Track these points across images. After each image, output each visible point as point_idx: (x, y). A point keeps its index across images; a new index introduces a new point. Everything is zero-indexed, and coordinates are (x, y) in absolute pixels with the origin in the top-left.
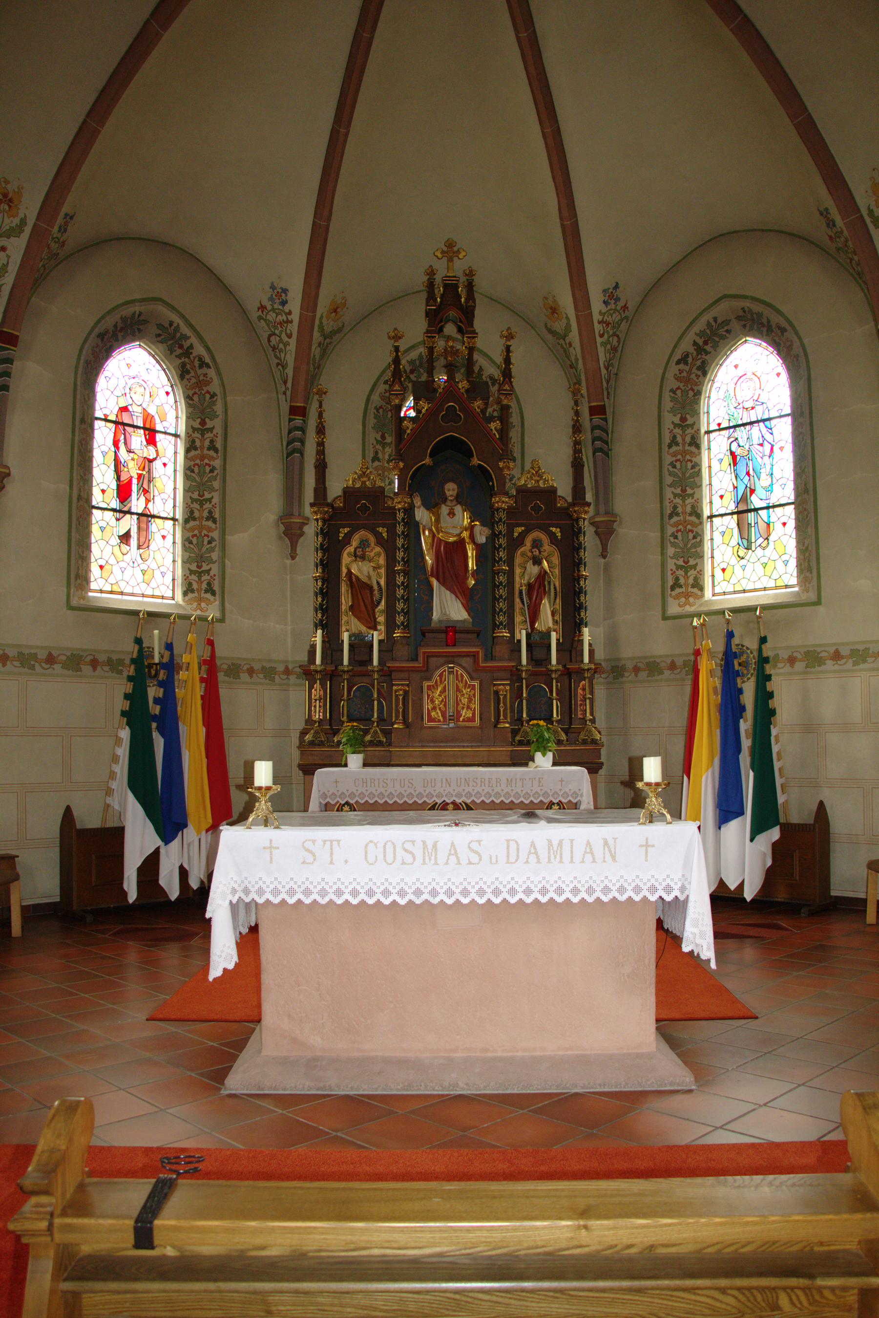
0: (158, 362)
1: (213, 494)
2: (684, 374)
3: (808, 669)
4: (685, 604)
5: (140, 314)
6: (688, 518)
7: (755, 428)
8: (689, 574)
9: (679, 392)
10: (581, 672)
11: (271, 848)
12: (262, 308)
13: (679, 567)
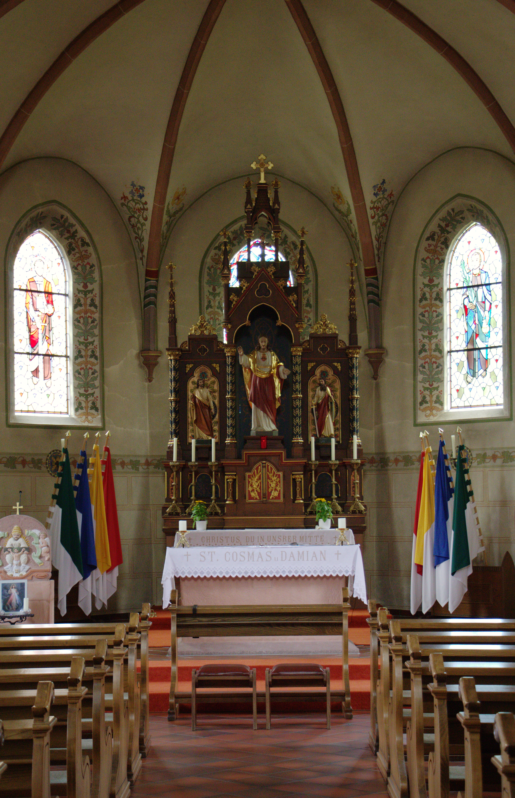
0: (51, 242)
1: (95, 338)
2: (432, 247)
3: (505, 464)
4: (430, 415)
5: (42, 213)
6: (433, 353)
7: (480, 290)
8: (433, 393)
9: (428, 261)
10: (351, 466)
11: (188, 555)
12: (125, 198)
13: (426, 389)
